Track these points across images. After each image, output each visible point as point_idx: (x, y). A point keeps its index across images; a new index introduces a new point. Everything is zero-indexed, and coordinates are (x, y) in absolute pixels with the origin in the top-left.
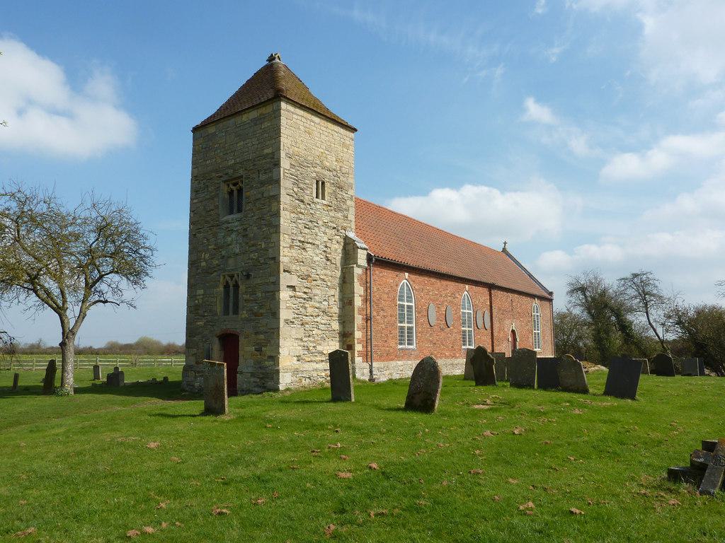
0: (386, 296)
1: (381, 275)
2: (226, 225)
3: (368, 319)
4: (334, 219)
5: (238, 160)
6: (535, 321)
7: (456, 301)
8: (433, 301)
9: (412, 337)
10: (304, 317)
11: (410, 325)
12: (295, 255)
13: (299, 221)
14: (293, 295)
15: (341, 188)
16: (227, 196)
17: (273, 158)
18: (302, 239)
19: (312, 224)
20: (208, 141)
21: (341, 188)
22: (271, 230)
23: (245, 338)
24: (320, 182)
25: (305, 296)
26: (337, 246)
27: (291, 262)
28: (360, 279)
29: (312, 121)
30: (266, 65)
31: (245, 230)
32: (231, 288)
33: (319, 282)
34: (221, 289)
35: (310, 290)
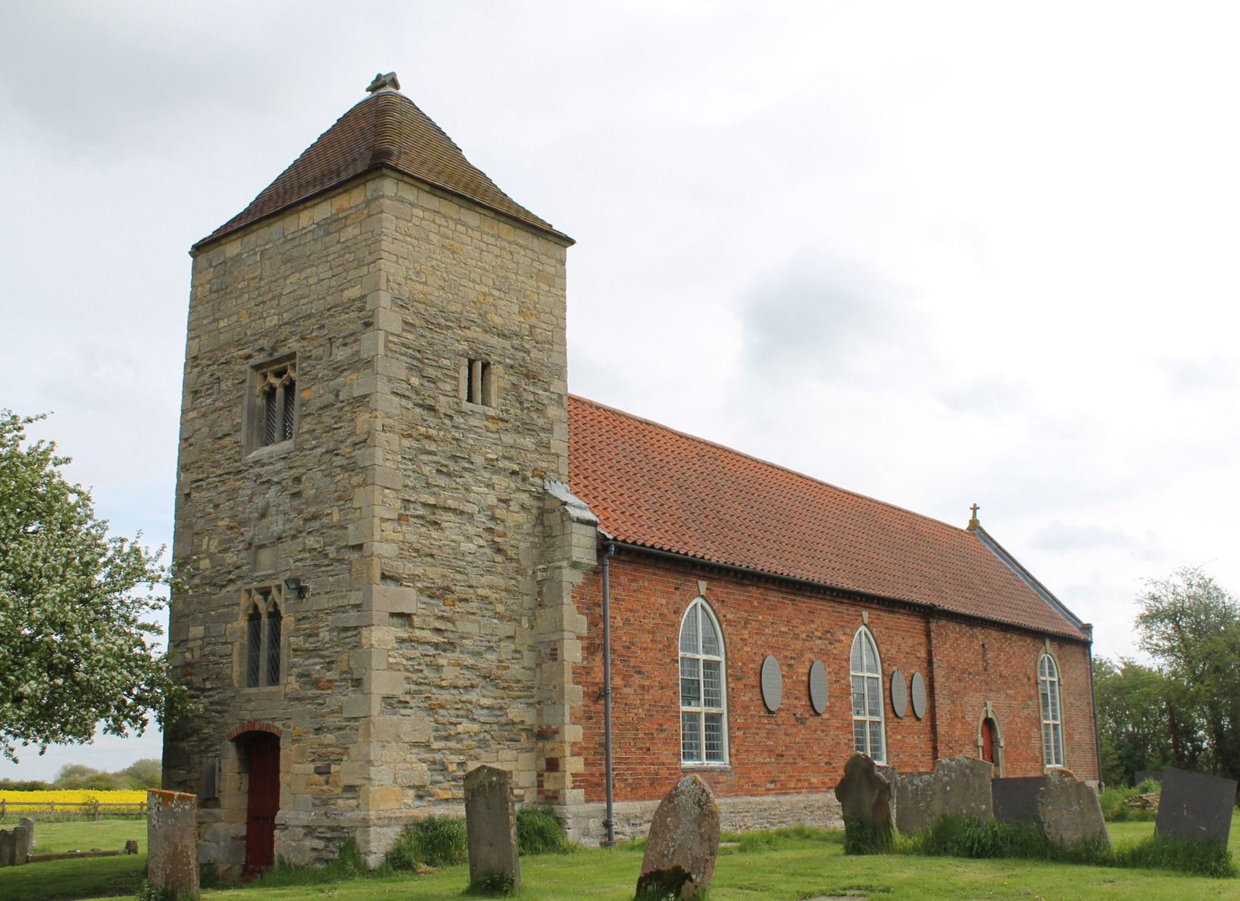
0: (647, 638)
1: (634, 586)
2: (257, 470)
3: (600, 695)
4: (513, 452)
5: (286, 316)
6: (1045, 695)
7: (836, 650)
8: (776, 649)
9: (719, 738)
10: (434, 690)
11: (714, 710)
12: (411, 538)
13: (424, 457)
14: (405, 635)
15: (531, 376)
16: (260, 402)
17: (361, 309)
18: (432, 501)
19: (456, 464)
20: (224, 275)
21: (531, 376)
22: (356, 480)
23: (294, 741)
24: (479, 365)
25: (436, 638)
26: (521, 517)
27: (400, 557)
28: (579, 594)
29: (458, 222)
30: (366, 102)
31: (298, 480)
32: (265, 620)
33: (474, 606)
34: (242, 623)
35: (450, 626)
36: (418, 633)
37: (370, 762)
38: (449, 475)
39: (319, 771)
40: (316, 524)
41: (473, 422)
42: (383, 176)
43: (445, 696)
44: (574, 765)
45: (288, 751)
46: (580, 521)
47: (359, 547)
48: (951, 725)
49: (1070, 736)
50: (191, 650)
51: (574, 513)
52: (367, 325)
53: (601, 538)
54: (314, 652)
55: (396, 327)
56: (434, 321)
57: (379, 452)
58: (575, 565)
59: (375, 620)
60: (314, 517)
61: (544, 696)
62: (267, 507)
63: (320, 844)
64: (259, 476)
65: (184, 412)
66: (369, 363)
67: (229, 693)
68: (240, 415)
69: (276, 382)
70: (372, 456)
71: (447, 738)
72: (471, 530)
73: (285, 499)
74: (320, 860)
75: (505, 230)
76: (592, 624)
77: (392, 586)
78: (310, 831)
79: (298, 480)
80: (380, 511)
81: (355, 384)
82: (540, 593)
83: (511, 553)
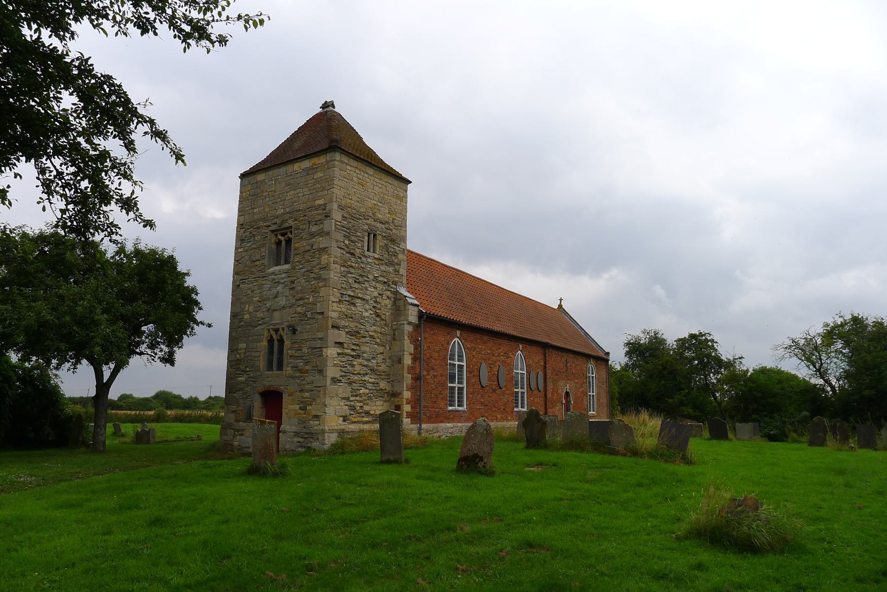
0: (436, 355)
3: (417, 378)
7: (508, 361)
11: (461, 386)
12: (344, 310)
15: (393, 241)
16: (274, 246)
17: (324, 209)
21: (393, 241)
22: (320, 284)
25: (353, 353)
26: (387, 302)
28: (410, 336)
29: (365, 172)
31: (293, 282)
32: (276, 342)
36: (346, 351)
37: (326, 406)
38: (359, 283)
39: (301, 409)
40: (301, 302)
41: (369, 260)
42: (335, 151)
43: (356, 378)
44: (407, 408)
45: (286, 399)
46: (412, 304)
47: (322, 313)
48: (553, 394)
49: (599, 400)
50: (240, 354)
51: (410, 301)
52: (327, 216)
53: (420, 312)
54: (300, 357)
55: (339, 218)
56: (351, 215)
57: (332, 274)
58: (410, 323)
59: (329, 345)
60: (301, 299)
61: (393, 377)
62: (278, 293)
63: (301, 440)
64: (274, 279)
65: (236, 249)
66: (328, 234)
67: (258, 373)
68: (264, 251)
69: (282, 238)
70: (329, 274)
71: (356, 396)
72: (367, 307)
73: (287, 290)
74: (302, 447)
75: (383, 176)
76: (415, 348)
77: (336, 331)
78: (296, 434)
79: (293, 282)
80: (332, 298)
81: (322, 242)
82: (394, 335)
83: (383, 317)
